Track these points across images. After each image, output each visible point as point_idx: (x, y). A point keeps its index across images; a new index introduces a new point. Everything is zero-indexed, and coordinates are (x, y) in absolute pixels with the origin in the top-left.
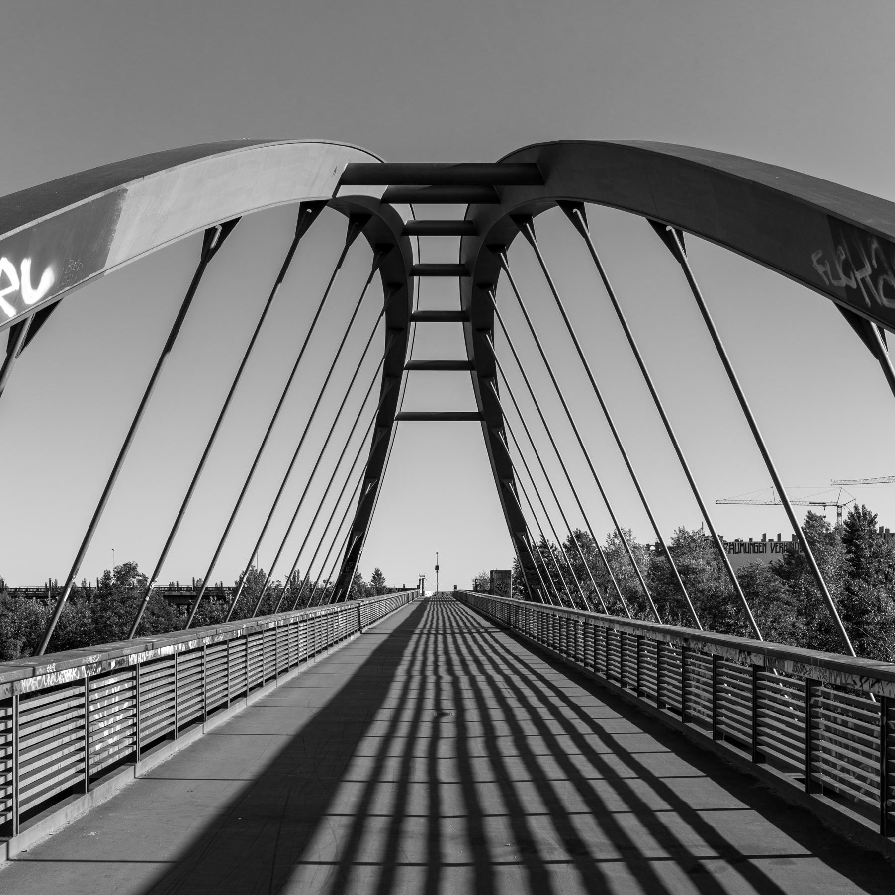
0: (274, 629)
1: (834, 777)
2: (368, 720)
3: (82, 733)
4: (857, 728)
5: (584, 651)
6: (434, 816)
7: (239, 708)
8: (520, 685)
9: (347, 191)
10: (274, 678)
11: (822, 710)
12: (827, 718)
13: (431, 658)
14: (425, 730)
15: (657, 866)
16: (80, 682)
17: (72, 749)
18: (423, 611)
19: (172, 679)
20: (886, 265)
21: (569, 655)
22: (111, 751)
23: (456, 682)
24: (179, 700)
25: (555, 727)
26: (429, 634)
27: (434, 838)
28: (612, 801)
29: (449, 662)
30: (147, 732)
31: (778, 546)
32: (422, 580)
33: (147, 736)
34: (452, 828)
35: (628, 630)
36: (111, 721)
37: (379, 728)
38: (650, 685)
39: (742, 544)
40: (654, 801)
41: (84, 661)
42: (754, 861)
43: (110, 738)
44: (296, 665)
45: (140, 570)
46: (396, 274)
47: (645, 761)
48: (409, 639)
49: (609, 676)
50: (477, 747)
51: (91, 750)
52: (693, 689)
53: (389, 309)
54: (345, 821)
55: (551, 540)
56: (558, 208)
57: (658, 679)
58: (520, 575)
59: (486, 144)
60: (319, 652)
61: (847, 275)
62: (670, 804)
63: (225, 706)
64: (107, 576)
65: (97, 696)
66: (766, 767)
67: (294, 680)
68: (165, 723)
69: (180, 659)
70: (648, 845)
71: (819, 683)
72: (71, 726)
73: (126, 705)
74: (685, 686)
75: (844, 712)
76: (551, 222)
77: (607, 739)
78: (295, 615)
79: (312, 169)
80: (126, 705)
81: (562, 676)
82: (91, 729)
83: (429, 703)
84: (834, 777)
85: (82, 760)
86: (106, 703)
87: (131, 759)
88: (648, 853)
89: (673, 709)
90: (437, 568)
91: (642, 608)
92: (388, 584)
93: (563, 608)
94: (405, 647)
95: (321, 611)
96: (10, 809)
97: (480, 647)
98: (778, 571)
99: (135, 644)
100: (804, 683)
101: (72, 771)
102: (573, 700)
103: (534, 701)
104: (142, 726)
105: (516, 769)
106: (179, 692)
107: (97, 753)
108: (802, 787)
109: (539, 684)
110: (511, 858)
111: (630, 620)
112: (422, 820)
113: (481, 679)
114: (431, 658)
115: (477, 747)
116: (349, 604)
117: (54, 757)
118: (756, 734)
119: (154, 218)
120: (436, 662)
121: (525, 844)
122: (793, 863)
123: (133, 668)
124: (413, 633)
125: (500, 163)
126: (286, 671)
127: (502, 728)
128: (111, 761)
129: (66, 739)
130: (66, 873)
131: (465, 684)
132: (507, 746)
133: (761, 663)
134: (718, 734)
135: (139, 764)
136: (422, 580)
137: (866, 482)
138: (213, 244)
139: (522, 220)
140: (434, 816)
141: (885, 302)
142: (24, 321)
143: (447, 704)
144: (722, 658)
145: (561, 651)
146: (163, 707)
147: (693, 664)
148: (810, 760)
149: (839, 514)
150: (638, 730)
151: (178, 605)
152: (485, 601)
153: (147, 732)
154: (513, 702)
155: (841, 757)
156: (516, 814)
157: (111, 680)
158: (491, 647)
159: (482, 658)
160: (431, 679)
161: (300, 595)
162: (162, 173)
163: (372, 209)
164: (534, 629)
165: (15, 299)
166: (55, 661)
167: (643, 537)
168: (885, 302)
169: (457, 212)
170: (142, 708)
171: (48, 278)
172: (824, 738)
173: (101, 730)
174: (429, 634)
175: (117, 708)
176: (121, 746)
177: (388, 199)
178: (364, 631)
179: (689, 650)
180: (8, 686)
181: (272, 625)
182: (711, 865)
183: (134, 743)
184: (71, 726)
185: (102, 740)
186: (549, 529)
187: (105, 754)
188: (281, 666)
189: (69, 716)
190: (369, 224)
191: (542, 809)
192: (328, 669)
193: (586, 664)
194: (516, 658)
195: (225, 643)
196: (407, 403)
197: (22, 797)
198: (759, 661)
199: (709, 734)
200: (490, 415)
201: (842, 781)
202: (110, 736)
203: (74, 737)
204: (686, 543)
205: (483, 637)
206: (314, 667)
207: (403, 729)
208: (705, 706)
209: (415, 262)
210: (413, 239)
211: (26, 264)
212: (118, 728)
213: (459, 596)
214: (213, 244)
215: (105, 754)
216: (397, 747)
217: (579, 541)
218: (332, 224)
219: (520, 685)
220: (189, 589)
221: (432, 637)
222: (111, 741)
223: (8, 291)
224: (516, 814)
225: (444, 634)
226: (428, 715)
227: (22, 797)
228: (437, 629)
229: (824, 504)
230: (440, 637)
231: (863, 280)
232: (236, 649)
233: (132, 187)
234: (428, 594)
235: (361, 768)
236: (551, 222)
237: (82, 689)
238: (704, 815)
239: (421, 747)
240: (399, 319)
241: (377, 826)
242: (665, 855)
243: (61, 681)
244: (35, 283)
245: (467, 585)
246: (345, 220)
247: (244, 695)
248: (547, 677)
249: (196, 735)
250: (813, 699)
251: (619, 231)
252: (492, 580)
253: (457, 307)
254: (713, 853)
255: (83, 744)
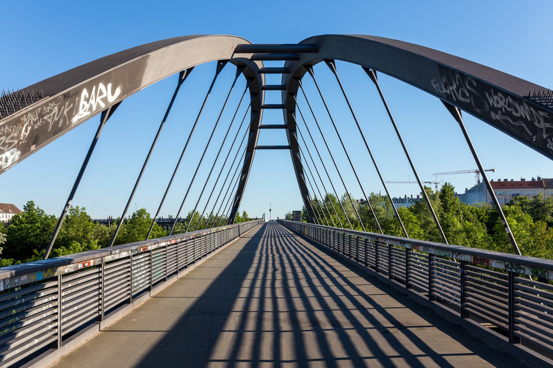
0: (205, 235)
1: (441, 294)
2: (246, 273)
3: (129, 278)
4: (451, 274)
5: (334, 244)
6: (276, 311)
7: (191, 268)
8: (307, 258)
9: (237, 56)
10: (205, 255)
11: (435, 266)
12: (438, 270)
13: (269, 247)
14: (269, 276)
15: (369, 331)
16: (128, 257)
17: (125, 285)
18: (264, 228)
19: (165, 256)
20: (462, 84)
21: (327, 245)
22: (141, 286)
23: (281, 257)
24: (168, 265)
25: (323, 275)
26: (268, 237)
27: (276, 320)
28: (349, 305)
29: (277, 249)
30: (155, 278)
31: (411, 200)
32: (264, 215)
33: (155, 280)
34: (283, 316)
35: (353, 235)
36: (141, 273)
37: (250, 276)
38: (362, 257)
39: (396, 199)
40: (367, 305)
41: (130, 248)
42: (409, 329)
43: (140, 281)
44: (214, 250)
45: (147, 212)
46: (256, 89)
47: (361, 288)
48: (260, 239)
49: (344, 254)
50: (291, 283)
51: (133, 285)
52: (380, 259)
53: (252, 104)
54: (239, 314)
55: (319, 198)
56: (323, 63)
57: (365, 254)
58: (305, 212)
59: (293, 37)
60: (223, 245)
61: (446, 88)
62: (373, 306)
63: (186, 267)
64: (134, 215)
65: (135, 263)
66: (412, 290)
67: (213, 256)
68: (162, 274)
69: (168, 248)
70: (365, 323)
71: (434, 255)
72: (125, 276)
73: (147, 267)
74: (377, 257)
75: (445, 267)
76: (321, 68)
77: (345, 279)
78: (214, 230)
79: (224, 47)
80: (147, 267)
81: (324, 254)
82: (133, 277)
83: (270, 266)
84: (441, 294)
85: (129, 290)
86: (139, 266)
87: (149, 289)
88: (365, 326)
89: (372, 267)
90: (270, 210)
91: (356, 226)
92: (249, 216)
93: (324, 226)
94: (259, 242)
95: (224, 228)
96: (100, 310)
97: (290, 242)
98: (411, 210)
99: (150, 242)
100: (428, 255)
101: (125, 294)
102: (330, 263)
103: (314, 264)
104: (153, 275)
105: (308, 292)
106: (168, 262)
107: (135, 287)
108: (428, 298)
109: (315, 257)
110: (309, 329)
111: (353, 230)
112: (270, 313)
113: (291, 255)
114: (269, 247)
115: (291, 283)
116: (235, 225)
117: (118, 288)
118: (407, 277)
119: (160, 67)
120: (272, 249)
121: (314, 323)
122: (425, 329)
123: (149, 251)
124: (261, 237)
125: (300, 44)
126: (210, 252)
127: (301, 275)
128: (140, 290)
129: (123, 281)
130: (124, 337)
131: (284, 257)
132: (304, 283)
133: (409, 248)
134: (391, 277)
135: (152, 291)
136: (264, 215)
137: (447, 173)
138: (183, 78)
139: (308, 67)
140: (276, 311)
141: (462, 99)
142: (107, 109)
143: (278, 266)
144: (392, 246)
145: (324, 244)
146: (162, 268)
147: (380, 248)
148: (431, 287)
149: (436, 187)
150: (357, 276)
151: (163, 226)
152: (292, 223)
153: (155, 278)
154: (305, 265)
155: (444, 285)
156: (309, 310)
157: (141, 257)
158: (294, 242)
159: (291, 247)
160: (270, 256)
161: (214, 222)
162: (164, 49)
163: (247, 63)
164: (312, 235)
165: (105, 100)
166: (119, 248)
167: (357, 195)
168: (462, 99)
169: (281, 64)
170: (153, 268)
171: (118, 91)
172: (436, 278)
173: (137, 277)
174: (268, 237)
175: (143, 268)
176: (145, 284)
177: (253, 59)
178: (241, 236)
179: (378, 242)
180: (100, 259)
181: (204, 234)
182: (392, 331)
183: (150, 283)
184: (125, 276)
185: (137, 281)
186: (317, 193)
187: (138, 287)
188: (208, 251)
189: (124, 271)
190: (245, 69)
191: (320, 308)
192: (227, 252)
193: (334, 249)
194: (305, 247)
195: (186, 241)
196: (259, 142)
197: (105, 305)
198: (408, 246)
199: (387, 277)
200: (294, 147)
201: (444, 295)
202: (140, 280)
203: (126, 280)
204: (374, 199)
205: (291, 238)
206: (221, 251)
207: (260, 276)
208: (385, 266)
209: (263, 84)
210: (263, 75)
211: (110, 86)
212: (143, 276)
213: (279, 222)
214: (183, 78)
215: (138, 287)
216: (258, 284)
217: (328, 198)
218: (231, 68)
219: (307, 258)
220: (167, 219)
221: (269, 239)
222: (140, 282)
223: (102, 97)
224: (309, 310)
225: (274, 237)
226: (270, 270)
227: (105, 305)
228: (271, 235)
229: (430, 183)
230: (273, 239)
231: (453, 90)
232: (190, 244)
233: (152, 54)
234: (267, 221)
235: (244, 292)
236: (321, 68)
237: (129, 260)
238: (387, 310)
239: (268, 283)
240: (256, 108)
241: (252, 316)
242: (372, 326)
243: (121, 257)
244: (113, 93)
245: (282, 217)
246: (235, 68)
247: (193, 262)
248: (318, 254)
249: (174, 279)
250: (432, 262)
251: (350, 71)
252: (293, 215)
253: (280, 102)
254: (392, 326)
255: (129, 283)
